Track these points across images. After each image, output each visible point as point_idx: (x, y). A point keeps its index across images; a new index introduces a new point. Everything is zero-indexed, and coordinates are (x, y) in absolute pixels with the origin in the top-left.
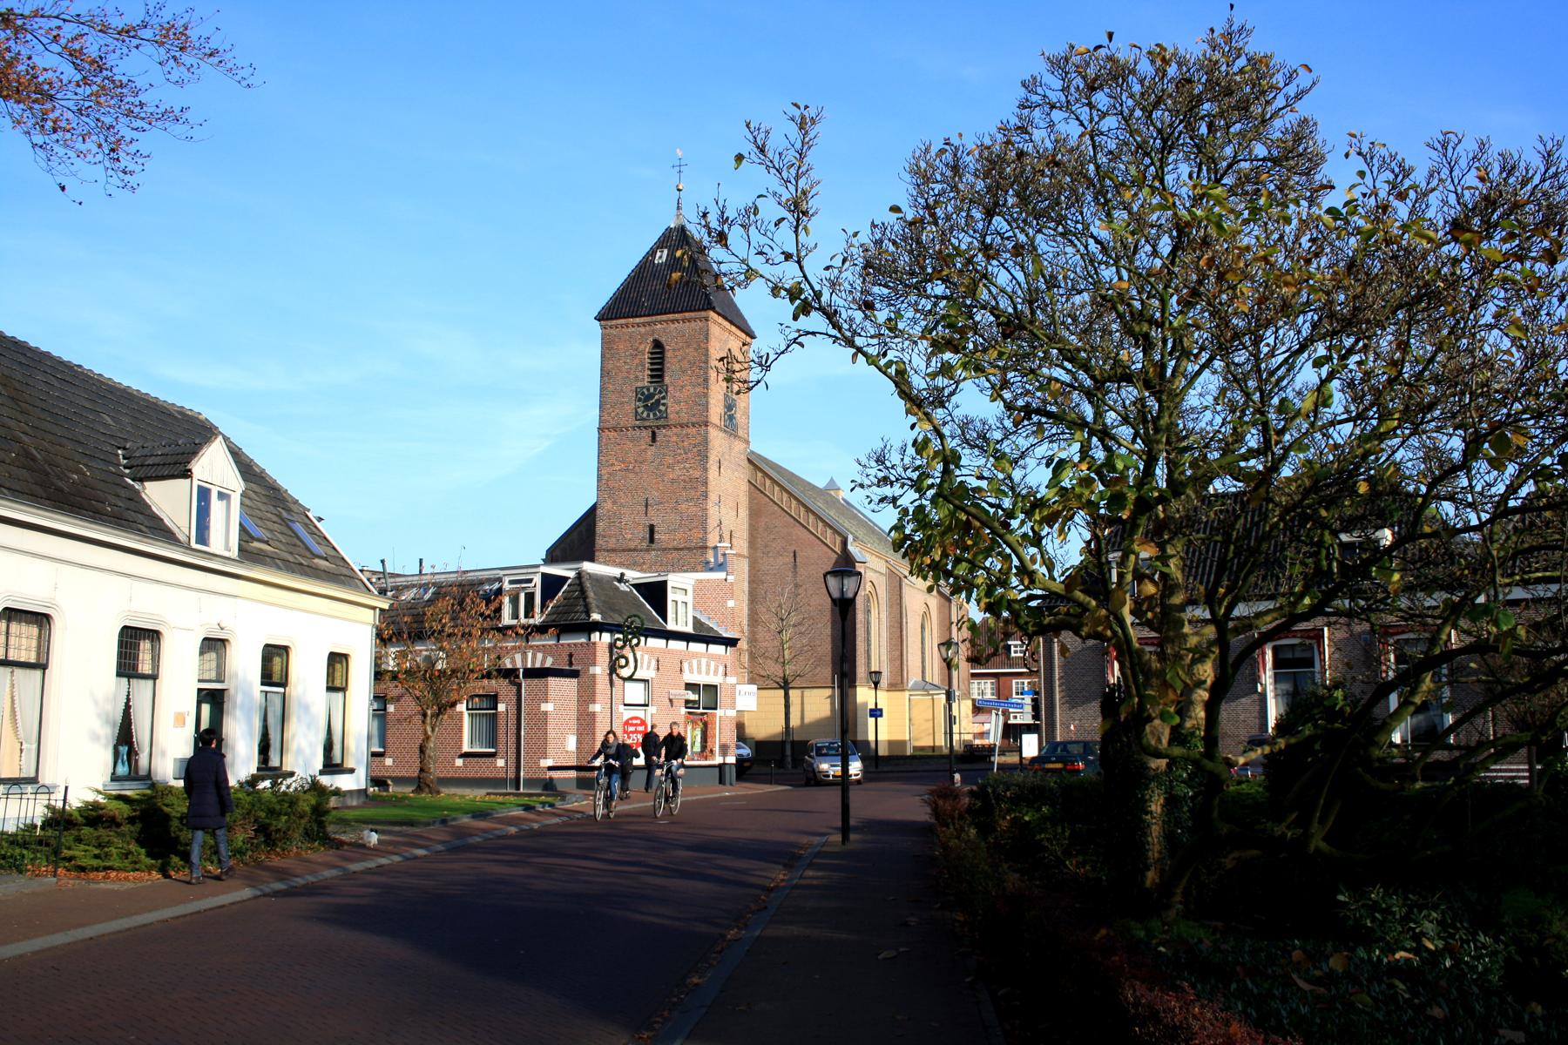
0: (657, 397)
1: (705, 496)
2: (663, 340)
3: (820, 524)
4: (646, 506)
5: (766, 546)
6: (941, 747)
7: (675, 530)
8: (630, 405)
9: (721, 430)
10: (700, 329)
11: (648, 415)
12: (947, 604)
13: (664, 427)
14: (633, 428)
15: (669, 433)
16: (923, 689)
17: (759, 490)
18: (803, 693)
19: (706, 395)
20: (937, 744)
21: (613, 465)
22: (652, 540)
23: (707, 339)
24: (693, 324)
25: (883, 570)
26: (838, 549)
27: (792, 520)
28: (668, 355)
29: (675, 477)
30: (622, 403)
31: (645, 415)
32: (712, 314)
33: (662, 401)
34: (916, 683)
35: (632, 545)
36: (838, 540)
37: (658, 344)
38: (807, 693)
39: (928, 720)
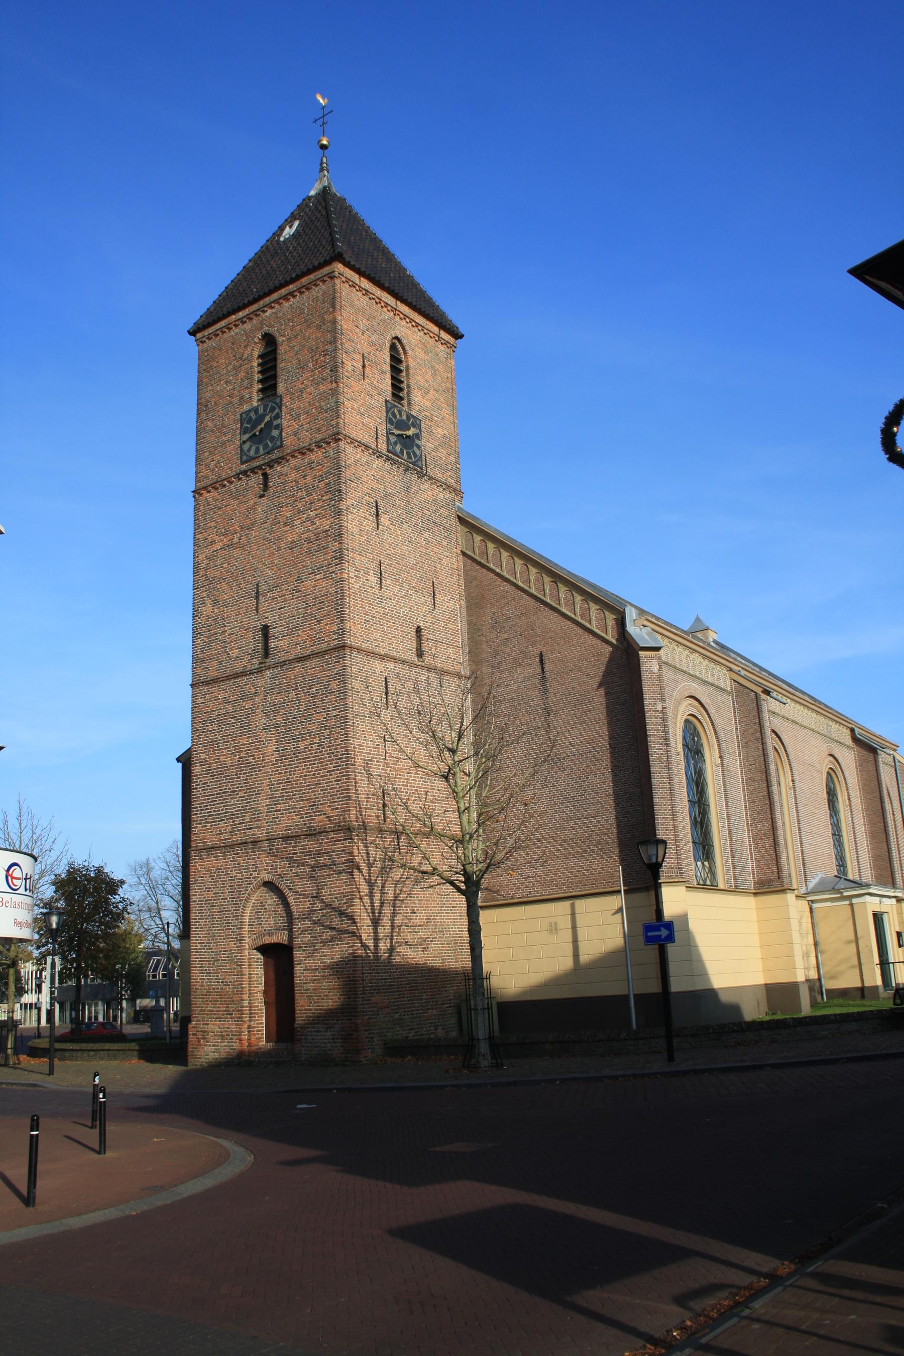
0: (267, 419)
1: (340, 557)
2: (274, 331)
3: (578, 598)
4: (257, 598)
5: (496, 653)
6: (876, 988)
7: (297, 628)
8: (233, 439)
9: (377, 454)
10: (324, 293)
11: (257, 451)
12: (871, 756)
13: (278, 461)
14: (237, 476)
15: (286, 469)
16: (834, 890)
17: (479, 564)
18: (573, 906)
19: (335, 392)
20: (867, 984)
21: (213, 542)
22: (266, 653)
23: (334, 306)
24: (315, 291)
25: (727, 685)
26: (611, 637)
27: (532, 602)
28: (282, 349)
29: (296, 537)
30: (224, 443)
31: (252, 453)
32: (339, 267)
33: (275, 423)
34: (822, 881)
35: (239, 667)
36: (611, 618)
37: (270, 340)
38: (580, 904)
39: (849, 942)
